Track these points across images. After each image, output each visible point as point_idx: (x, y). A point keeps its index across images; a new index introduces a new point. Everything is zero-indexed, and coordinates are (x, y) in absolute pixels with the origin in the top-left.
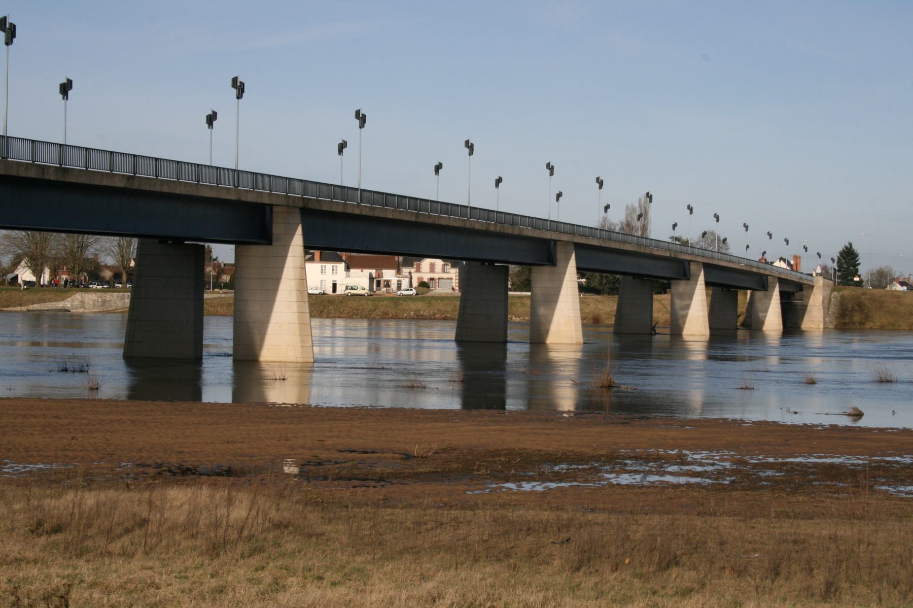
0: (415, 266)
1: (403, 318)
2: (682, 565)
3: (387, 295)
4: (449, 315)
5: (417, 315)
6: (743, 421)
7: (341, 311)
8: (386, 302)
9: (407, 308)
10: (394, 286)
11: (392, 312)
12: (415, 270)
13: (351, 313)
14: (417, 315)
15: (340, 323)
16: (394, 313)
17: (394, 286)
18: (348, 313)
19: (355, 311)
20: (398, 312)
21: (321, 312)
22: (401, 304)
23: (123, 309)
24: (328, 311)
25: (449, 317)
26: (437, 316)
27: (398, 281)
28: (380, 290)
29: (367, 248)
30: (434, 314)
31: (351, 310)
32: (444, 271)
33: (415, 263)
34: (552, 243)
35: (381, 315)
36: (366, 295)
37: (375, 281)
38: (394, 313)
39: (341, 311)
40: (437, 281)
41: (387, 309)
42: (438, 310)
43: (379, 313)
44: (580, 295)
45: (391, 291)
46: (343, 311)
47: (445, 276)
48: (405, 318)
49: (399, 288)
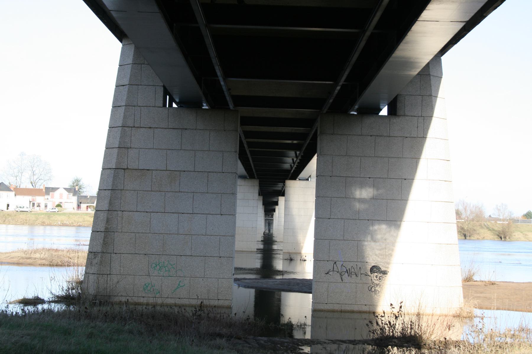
0: (50, 195)
1: (54, 225)
2: (222, 349)
3: (39, 212)
4: (81, 224)
5: (63, 224)
6: (312, 302)
7: (16, 220)
8: (43, 216)
9: (56, 219)
10: (42, 206)
11: (47, 222)
12: (50, 197)
13: (22, 222)
14: (63, 224)
15: (11, 227)
16: (48, 222)
17: (42, 206)
18: (21, 222)
19: (25, 221)
20: (51, 221)
21: (4, 221)
22: (53, 217)
23: (225, 86)
24: (8, 220)
25: (81, 225)
26: (75, 224)
27: (45, 203)
28: (34, 209)
29: (376, 264)
30: (72, 223)
31: (22, 220)
32: (68, 198)
33: (51, 193)
34: (261, 194)
35: (41, 224)
36: (29, 211)
37: (31, 203)
38: (48, 222)
39: (16, 220)
40: (64, 204)
41: (44, 220)
42: (74, 221)
43: (40, 222)
44: (303, 245)
45: (41, 209)
46: (18, 221)
47: (69, 201)
48: (56, 225)
49: (46, 206)
